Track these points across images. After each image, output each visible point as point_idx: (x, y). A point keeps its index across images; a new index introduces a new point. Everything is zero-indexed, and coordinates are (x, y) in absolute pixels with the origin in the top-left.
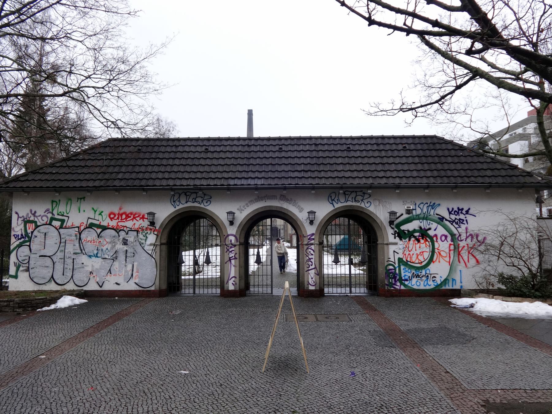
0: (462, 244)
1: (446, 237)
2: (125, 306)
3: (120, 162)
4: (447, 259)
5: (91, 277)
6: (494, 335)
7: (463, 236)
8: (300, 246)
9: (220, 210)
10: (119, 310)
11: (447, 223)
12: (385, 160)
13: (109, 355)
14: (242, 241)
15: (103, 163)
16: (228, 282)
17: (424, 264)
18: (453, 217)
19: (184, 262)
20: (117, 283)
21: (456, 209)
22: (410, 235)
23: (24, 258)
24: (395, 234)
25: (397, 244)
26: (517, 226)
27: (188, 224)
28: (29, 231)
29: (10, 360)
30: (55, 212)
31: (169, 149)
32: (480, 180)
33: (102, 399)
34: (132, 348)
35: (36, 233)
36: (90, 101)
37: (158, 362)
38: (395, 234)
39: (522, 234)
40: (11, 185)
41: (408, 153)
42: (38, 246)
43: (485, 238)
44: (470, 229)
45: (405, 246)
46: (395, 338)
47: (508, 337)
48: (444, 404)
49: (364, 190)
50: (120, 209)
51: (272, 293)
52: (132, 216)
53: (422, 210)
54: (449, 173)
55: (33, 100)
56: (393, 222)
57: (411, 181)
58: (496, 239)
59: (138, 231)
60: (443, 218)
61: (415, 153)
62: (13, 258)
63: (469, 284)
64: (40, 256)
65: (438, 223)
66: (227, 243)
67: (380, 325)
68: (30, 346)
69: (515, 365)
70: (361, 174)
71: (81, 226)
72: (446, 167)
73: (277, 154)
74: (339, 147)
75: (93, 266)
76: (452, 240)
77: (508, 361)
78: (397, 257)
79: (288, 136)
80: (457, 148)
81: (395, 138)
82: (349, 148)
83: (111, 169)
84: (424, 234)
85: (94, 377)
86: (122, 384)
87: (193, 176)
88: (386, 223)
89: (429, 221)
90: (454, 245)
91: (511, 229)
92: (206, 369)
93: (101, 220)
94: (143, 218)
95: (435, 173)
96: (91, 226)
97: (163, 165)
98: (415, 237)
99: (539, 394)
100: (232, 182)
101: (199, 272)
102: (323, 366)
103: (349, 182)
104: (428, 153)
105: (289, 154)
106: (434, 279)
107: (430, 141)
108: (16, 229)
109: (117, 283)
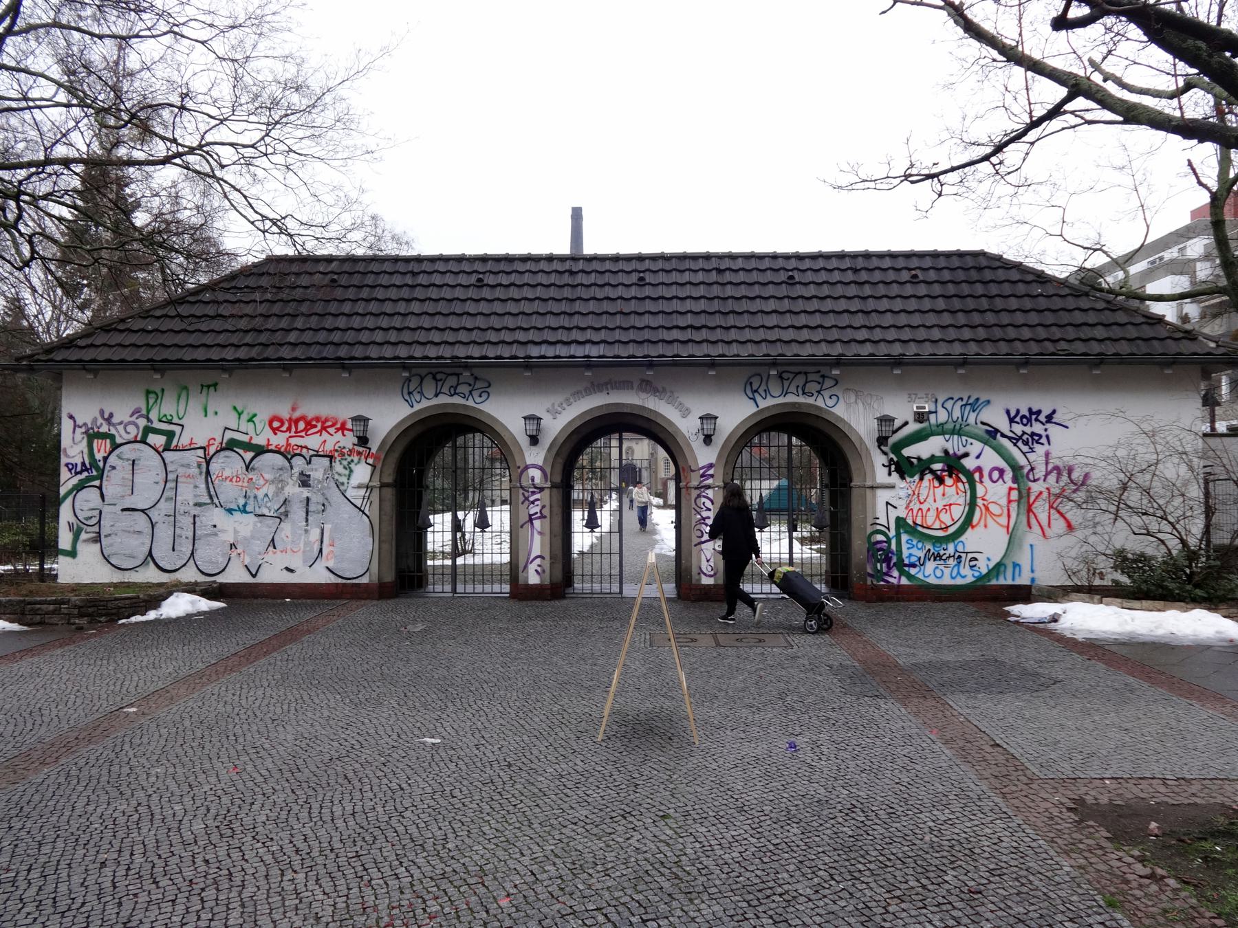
0: (1036, 488)
1: (1002, 472)
2: (307, 615)
3: (290, 309)
4: (1004, 520)
5: (234, 555)
6: (1101, 674)
7: (1040, 472)
8: (683, 491)
9: (508, 411)
10: (292, 623)
11: (1005, 442)
12: (871, 305)
13: (272, 708)
14: (558, 479)
15: (256, 309)
16: (526, 567)
17: (951, 530)
18: (1018, 429)
19: (431, 525)
20: (288, 569)
21: (1024, 412)
22: (922, 468)
23: (89, 514)
24: (889, 466)
25: (893, 487)
26: (1159, 448)
27: (440, 444)
28: (99, 456)
29: (61, 714)
30: (153, 415)
31: (397, 280)
32: (1079, 347)
33: (257, 789)
34: (321, 695)
35: (113, 460)
36: (227, 174)
37: (375, 721)
38: (889, 466)
39: (1169, 465)
40: (59, 356)
41: (922, 290)
42: (119, 489)
43: (1087, 476)
44: (1054, 454)
45: (910, 492)
46: (885, 679)
47: (1131, 680)
48: (987, 805)
49: (824, 370)
50: (294, 409)
51: (621, 592)
52: (319, 425)
53: (950, 414)
54: (1011, 333)
55: (102, 178)
56: (886, 438)
57: (928, 349)
58: (1111, 477)
59: (331, 458)
60: (997, 431)
61: (937, 289)
62: (65, 513)
63: (1050, 576)
64: (123, 510)
65: (985, 443)
66: (524, 484)
67: (853, 655)
68: (104, 689)
69: (1145, 731)
70: (818, 335)
71: (209, 445)
72: (1005, 319)
73: (633, 292)
74: (769, 276)
75: (236, 532)
76: (1015, 480)
77: (1129, 726)
78: (893, 514)
79: (659, 251)
80: (1030, 278)
81: (893, 255)
82: (791, 277)
83: (271, 323)
84: (953, 465)
85: (240, 748)
86: (300, 762)
87: (449, 336)
88: (870, 442)
89: (964, 438)
90: (1019, 490)
91: (1146, 454)
92: (477, 735)
93: (252, 433)
94: (343, 428)
95: (981, 333)
96: (231, 445)
97: (386, 314)
98: (932, 472)
99: (1195, 788)
100: (534, 351)
101: (465, 552)
102: (728, 732)
103: (790, 351)
104: (966, 289)
105: (661, 291)
106: (973, 563)
107: (970, 262)
108: (71, 452)
109: (288, 569)
